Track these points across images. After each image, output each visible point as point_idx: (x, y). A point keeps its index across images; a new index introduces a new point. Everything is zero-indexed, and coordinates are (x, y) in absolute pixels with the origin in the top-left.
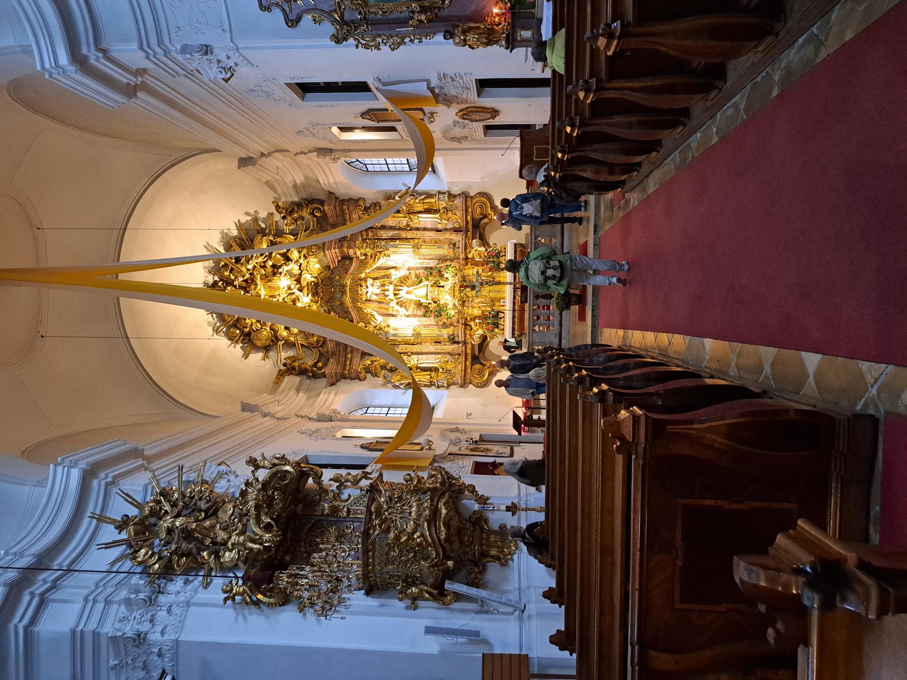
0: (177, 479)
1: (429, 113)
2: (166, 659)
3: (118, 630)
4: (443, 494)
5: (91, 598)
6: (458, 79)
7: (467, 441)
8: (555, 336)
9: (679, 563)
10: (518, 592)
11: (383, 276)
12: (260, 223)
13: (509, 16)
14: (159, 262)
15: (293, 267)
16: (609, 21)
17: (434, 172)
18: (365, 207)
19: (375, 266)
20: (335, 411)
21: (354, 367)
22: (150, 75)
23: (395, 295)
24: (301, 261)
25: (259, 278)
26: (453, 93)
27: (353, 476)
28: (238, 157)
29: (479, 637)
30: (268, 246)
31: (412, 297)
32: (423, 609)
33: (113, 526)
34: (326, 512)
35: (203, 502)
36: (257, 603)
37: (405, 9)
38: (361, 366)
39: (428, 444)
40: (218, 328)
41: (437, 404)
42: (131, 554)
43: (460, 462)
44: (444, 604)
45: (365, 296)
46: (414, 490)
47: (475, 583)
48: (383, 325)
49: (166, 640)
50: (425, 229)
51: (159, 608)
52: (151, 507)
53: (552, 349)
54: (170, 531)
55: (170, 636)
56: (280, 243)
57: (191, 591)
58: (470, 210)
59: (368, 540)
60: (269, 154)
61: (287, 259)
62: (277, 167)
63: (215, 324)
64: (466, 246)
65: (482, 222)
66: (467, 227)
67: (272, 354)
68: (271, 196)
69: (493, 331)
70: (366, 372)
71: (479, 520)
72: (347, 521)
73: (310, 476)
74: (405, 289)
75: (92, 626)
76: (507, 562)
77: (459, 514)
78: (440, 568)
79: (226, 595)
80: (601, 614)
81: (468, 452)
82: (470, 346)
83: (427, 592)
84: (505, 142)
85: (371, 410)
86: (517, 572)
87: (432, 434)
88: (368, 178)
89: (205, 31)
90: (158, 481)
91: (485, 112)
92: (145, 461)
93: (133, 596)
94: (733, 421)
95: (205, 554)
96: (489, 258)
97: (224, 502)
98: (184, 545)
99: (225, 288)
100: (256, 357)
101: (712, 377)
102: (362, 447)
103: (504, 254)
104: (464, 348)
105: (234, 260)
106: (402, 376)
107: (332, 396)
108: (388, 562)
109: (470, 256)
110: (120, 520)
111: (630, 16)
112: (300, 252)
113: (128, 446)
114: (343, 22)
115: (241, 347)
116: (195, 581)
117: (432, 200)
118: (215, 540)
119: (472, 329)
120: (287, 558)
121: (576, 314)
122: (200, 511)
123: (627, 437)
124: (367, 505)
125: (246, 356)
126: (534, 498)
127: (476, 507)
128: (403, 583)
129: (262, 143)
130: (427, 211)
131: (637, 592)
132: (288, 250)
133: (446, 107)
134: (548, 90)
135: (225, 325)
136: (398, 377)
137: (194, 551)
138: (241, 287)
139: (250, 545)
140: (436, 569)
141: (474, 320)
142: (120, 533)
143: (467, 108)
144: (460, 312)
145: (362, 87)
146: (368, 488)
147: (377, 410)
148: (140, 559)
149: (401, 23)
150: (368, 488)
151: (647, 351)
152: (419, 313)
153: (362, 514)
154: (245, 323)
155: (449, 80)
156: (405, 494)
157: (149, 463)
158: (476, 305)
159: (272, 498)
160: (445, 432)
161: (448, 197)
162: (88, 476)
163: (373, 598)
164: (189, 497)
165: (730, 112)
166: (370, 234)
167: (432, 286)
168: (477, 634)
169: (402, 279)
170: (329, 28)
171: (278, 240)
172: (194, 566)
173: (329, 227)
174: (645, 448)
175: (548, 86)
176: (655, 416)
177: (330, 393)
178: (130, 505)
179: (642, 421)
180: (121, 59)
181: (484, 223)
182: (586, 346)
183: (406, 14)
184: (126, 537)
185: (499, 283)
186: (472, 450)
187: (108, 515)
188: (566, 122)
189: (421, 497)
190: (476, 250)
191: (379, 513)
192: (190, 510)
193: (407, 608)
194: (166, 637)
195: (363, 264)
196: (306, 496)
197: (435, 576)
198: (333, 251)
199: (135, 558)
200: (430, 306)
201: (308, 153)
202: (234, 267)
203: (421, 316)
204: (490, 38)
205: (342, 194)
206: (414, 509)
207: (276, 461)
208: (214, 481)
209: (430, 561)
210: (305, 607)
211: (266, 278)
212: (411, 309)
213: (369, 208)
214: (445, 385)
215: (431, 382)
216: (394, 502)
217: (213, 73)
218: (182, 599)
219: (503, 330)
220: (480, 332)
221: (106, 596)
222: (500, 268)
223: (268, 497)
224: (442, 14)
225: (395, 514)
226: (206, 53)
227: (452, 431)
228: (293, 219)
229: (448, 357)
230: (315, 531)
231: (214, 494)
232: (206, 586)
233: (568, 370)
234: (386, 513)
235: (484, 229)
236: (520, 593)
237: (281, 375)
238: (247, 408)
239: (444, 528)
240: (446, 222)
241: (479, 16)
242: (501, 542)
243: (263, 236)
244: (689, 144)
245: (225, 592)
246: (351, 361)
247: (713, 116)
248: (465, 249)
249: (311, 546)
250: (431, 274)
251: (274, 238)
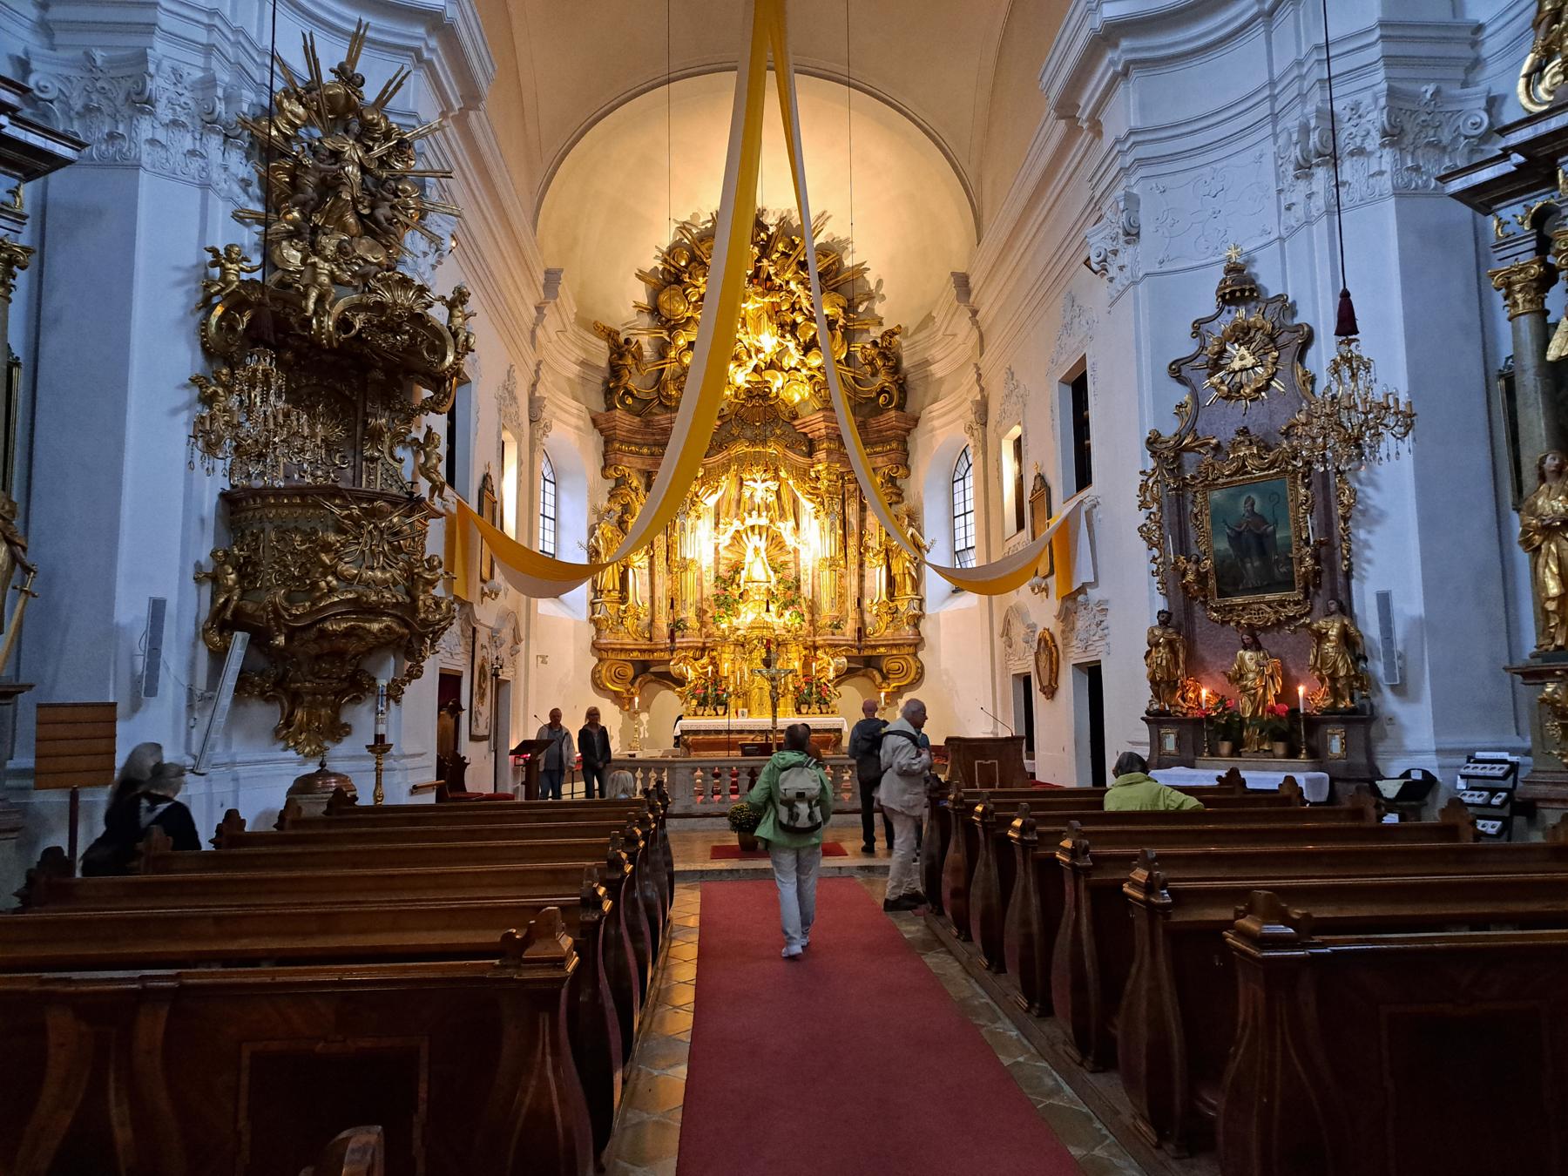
0: (428, 168)
1: (1046, 585)
2: (103, 147)
3: (158, 67)
4: (407, 625)
5: (217, 21)
6: (1100, 632)
7: (497, 658)
8: (686, 807)
9: (319, 1047)
10: (227, 760)
11: (782, 506)
12: (865, 304)
13: (1196, 714)
14: (796, 147)
15: (793, 358)
16: (1171, 885)
17: (953, 592)
18: (895, 478)
19: (799, 494)
20: (548, 427)
21: (625, 459)
22: (1094, 138)
23: (753, 528)
24: (804, 371)
25: (774, 300)
26: (1080, 624)
27: (435, 467)
28: (969, 273)
29: (146, 695)
30: (827, 316)
31: (749, 556)
32: (196, 593)
33: (344, 60)
34: (372, 421)
35: (388, 213)
36: (207, 305)
37: (1203, 548)
38: (627, 470)
39: (491, 592)
40: (689, 231)
41: (562, 601)
42: (296, 91)
43: (460, 649)
44: (205, 631)
45: (749, 477)
46: (413, 574)
47: (244, 684)
48: (701, 507)
49: (140, 148)
50: (862, 577)
51: (198, 136)
52: (378, 124)
53: (665, 807)
54: (336, 155)
55: (146, 155)
56: (834, 336)
57: (230, 190)
58: (895, 652)
59: (323, 496)
60: (975, 323)
61: (807, 348)
62: (955, 335)
63: (696, 226)
64: (836, 646)
66: (867, 647)
67: (646, 320)
68: (909, 322)
69: (694, 696)
70: (617, 479)
71: (358, 686)
72: (355, 457)
73: (435, 392)
74: (763, 544)
75: (165, 21)
76: (283, 739)
77: (370, 651)
78: (272, 623)
79: (222, 252)
80: (218, 920)
81: (478, 661)
83: (227, 601)
84: (1005, 709)
85: (550, 488)
86: (266, 758)
87: (509, 596)
88: (942, 482)
89: (1160, 231)
90: (424, 135)
91: (1050, 676)
92: (457, 113)
93: (220, 92)
94: (559, 1119)
95: (296, 214)
96: (817, 687)
97: (387, 247)
98: (311, 179)
99: (755, 244)
100: (641, 294)
101: (624, 1082)
102: (486, 478)
103: (824, 711)
104: (663, 647)
105: (802, 259)
106: (612, 540)
107: (574, 421)
108: (283, 532)
109: (820, 653)
110: (356, 72)
111: (1178, 917)
112: (819, 369)
113: (484, 85)
114: (1179, 450)
115: (656, 268)
116: (246, 198)
117: (909, 589)
118: (320, 232)
119: (696, 660)
120: (289, 355)
121: (725, 841)
122: (373, 207)
123: (528, 951)
124: (386, 494)
125: (641, 276)
126: (399, 783)
127: (383, 682)
128: (244, 558)
129: (993, 313)
130: (891, 581)
131: (268, 980)
132: (820, 349)
133: (1056, 614)
134: (1087, 783)
135: (693, 242)
136: (610, 535)
137: (300, 195)
138: (758, 270)
139: (314, 294)
140: (271, 616)
141: (711, 663)
142: (332, 71)
143: (1056, 646)
144: (725, 638)
145: (1083, 478)
146: (415, 495)
147: (550, 499)
148: (286, 104)
149: (1181, 544)
150: (415, 495)
151: (664, 970)
152: (722, 569)
153: (369, 483)
154: (697, 276)
155: (1098, 618)
156: (406, 557)
157: (456, 119)
158: (737, 667)
159: (396, 330)
160: (512, 621)
161: (915, 615)
162: (435, 21)
163: (217, 504)
164: (397, 188)
165: (1049, 1082)
166: (852, 487)
167: (768, 590)
168: (152, 690)
169: (779, 540)
170: (1170, 428)
171: (839, 333)
172: (273, 201)
173: (860, 419)
174: (512, 980)
175: (1095, 784)
176: (564, 992)
177: (579, 417)
178: (382, 88)
179: (555, 973)
180: (1114, 100)
182: (670, 864)
183: (1194, 551)
184: (325, 80)
185: (774, 707)
186: (482, 667)
187: (364, 51)
188: (1028, 819)
189: (401, 588)
190: (829, 664)
191: (372, 514)
192: (373, 189)
193: (198, 566)
194: (145, 148)
195: (802, 475)
196: (400, 386)
197: (257, 613)
198: (822, 425)
199: (287, 95)
200: (735, 586)
201: (980, 385)
202: (792, 259)
203: (717, 571)
204: (1163, 685)
205: (915, 439)
206: (379, 574)
207: (462, 338)
208: (424, 231)
209: (285, 604)
210: (200, 387)
211: (775, 311)
212: (730, 555)
213: (894, 485)
214: (597, 616)
215: (601, 591)
216: (391, 539)
217: (1098, 241)
218: (215, 176)
219: (696, 715)
220: (691, 675)
221: (218, 46)
222: (800, 705)
223: (400, 325)
224: (1196, 608)
225: (369, 542)
226: (1127, 234)
227: (516, 631)
228: (873, 359)
229: (647, 620)
230: (337, 402)
231: (402, 230)
232: (240, 217)
233: (632, 840)
234: (372, 526)
235: (864, 675)
236: (225, 764)
237: (609, 335)
238: (552, 279)
239: (346, 628)
240: (874, 612)
241: (1195, 666)
242: (318, 727)
243: (843, 308)
244: (1000, 1019)
245: (228, 249)
246: (637, 453)
247: (1042, 1056)
248: (831, 646)
249: (310, 396)
250: (789, 588)
251: (840, 327)
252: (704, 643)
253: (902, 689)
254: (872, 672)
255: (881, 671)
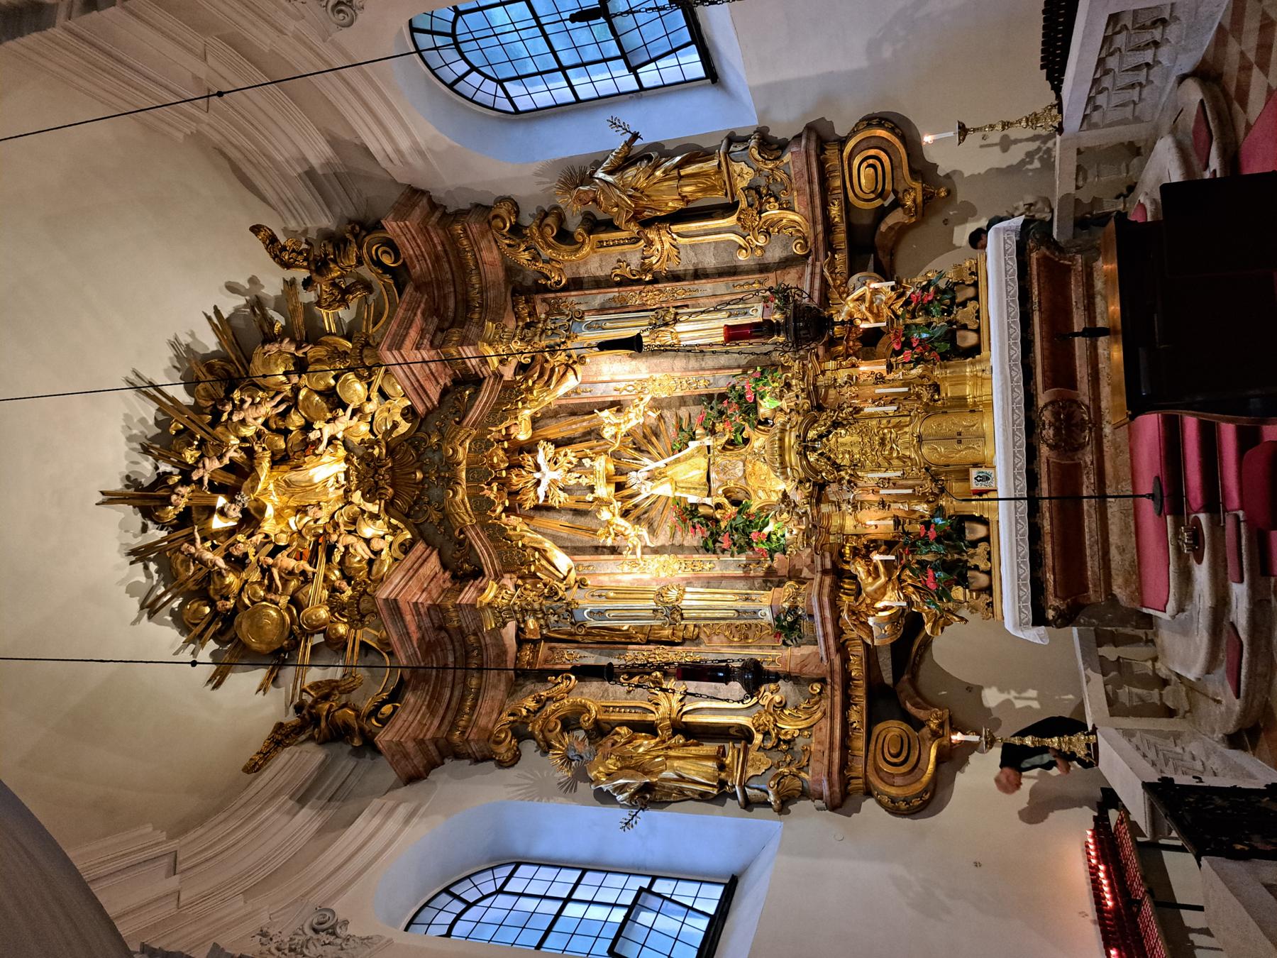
21: (483, 721)
45: (532, 495)
63: (153, 589)
65: (883, 228)
67: (288, 673)
69: (944, 594)
74: (648, 464)
82: (860, 650)
88: (519, 132)
100: (246, 681)
103: (970, 292)
106: (622, 758)
107: (392, 826)
125: (217, 681)
141: (867, 557)
152: (693, 539)
181: (891, 228)
195: (511, 394)
203: (696, 550)
214: (772, 798)
219: (989, 590)
220: (892, 600)
240: (762, 241)
252: (825, 572)
253: (916, 167)
254: (884, 235)
255: (882, 213)
